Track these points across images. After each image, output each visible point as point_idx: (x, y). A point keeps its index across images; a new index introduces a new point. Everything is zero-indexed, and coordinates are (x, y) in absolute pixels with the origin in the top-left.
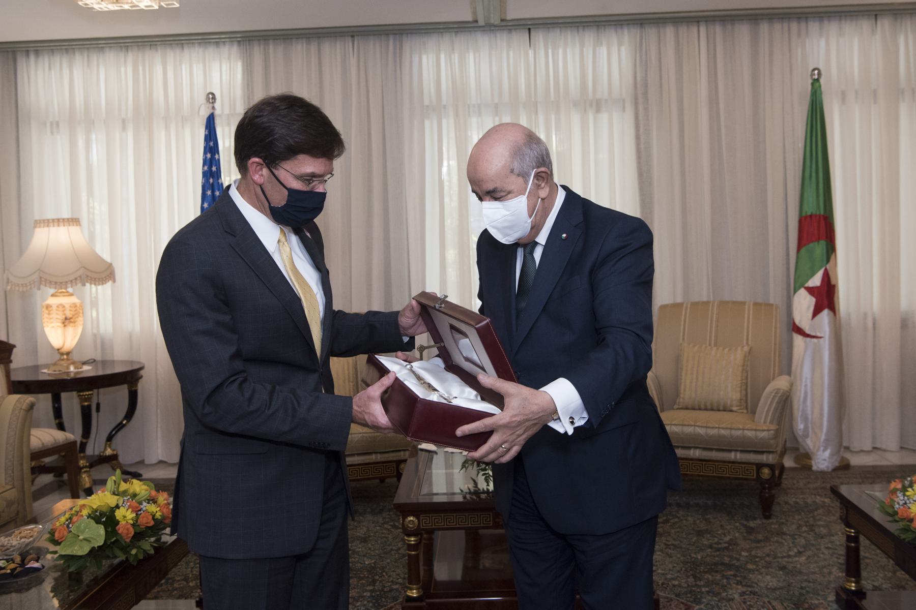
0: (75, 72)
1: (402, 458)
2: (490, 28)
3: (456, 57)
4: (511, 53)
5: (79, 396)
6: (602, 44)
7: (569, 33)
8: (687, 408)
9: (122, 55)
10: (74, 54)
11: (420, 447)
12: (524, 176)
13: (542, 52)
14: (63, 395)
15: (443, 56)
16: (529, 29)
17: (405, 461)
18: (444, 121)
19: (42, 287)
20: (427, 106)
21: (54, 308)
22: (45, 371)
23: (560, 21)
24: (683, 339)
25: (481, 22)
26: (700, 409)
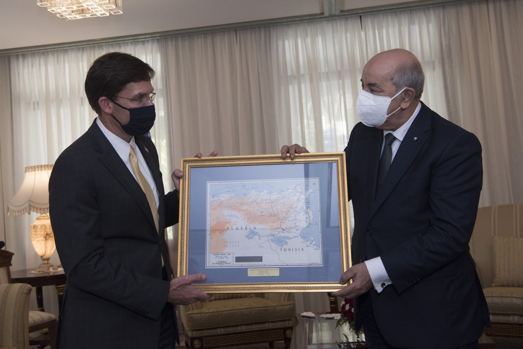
0: (49, 67)
1: (287, 326)
2: (332, 18)
3: (309, 40)
4: (348, 35)
5: (57, 288)
6: (414, 23)
7: (390, 17)
8: (503, 286)
9: (80, 54)
10: (48, 54)
11: (302, 314)
12: (398, 87)
13: (370, 33)
14: (44, 288)
15: (299, 41)
16: (360, 16)
17: (291, 328)
18: (303, 86)
19: (32, 212)
20: (290, 76)
21: (39, 227)
22: (33, 272)
23: (383, 9)
24: (494, 233)
25: (326, 14)
26: (514, 286)
